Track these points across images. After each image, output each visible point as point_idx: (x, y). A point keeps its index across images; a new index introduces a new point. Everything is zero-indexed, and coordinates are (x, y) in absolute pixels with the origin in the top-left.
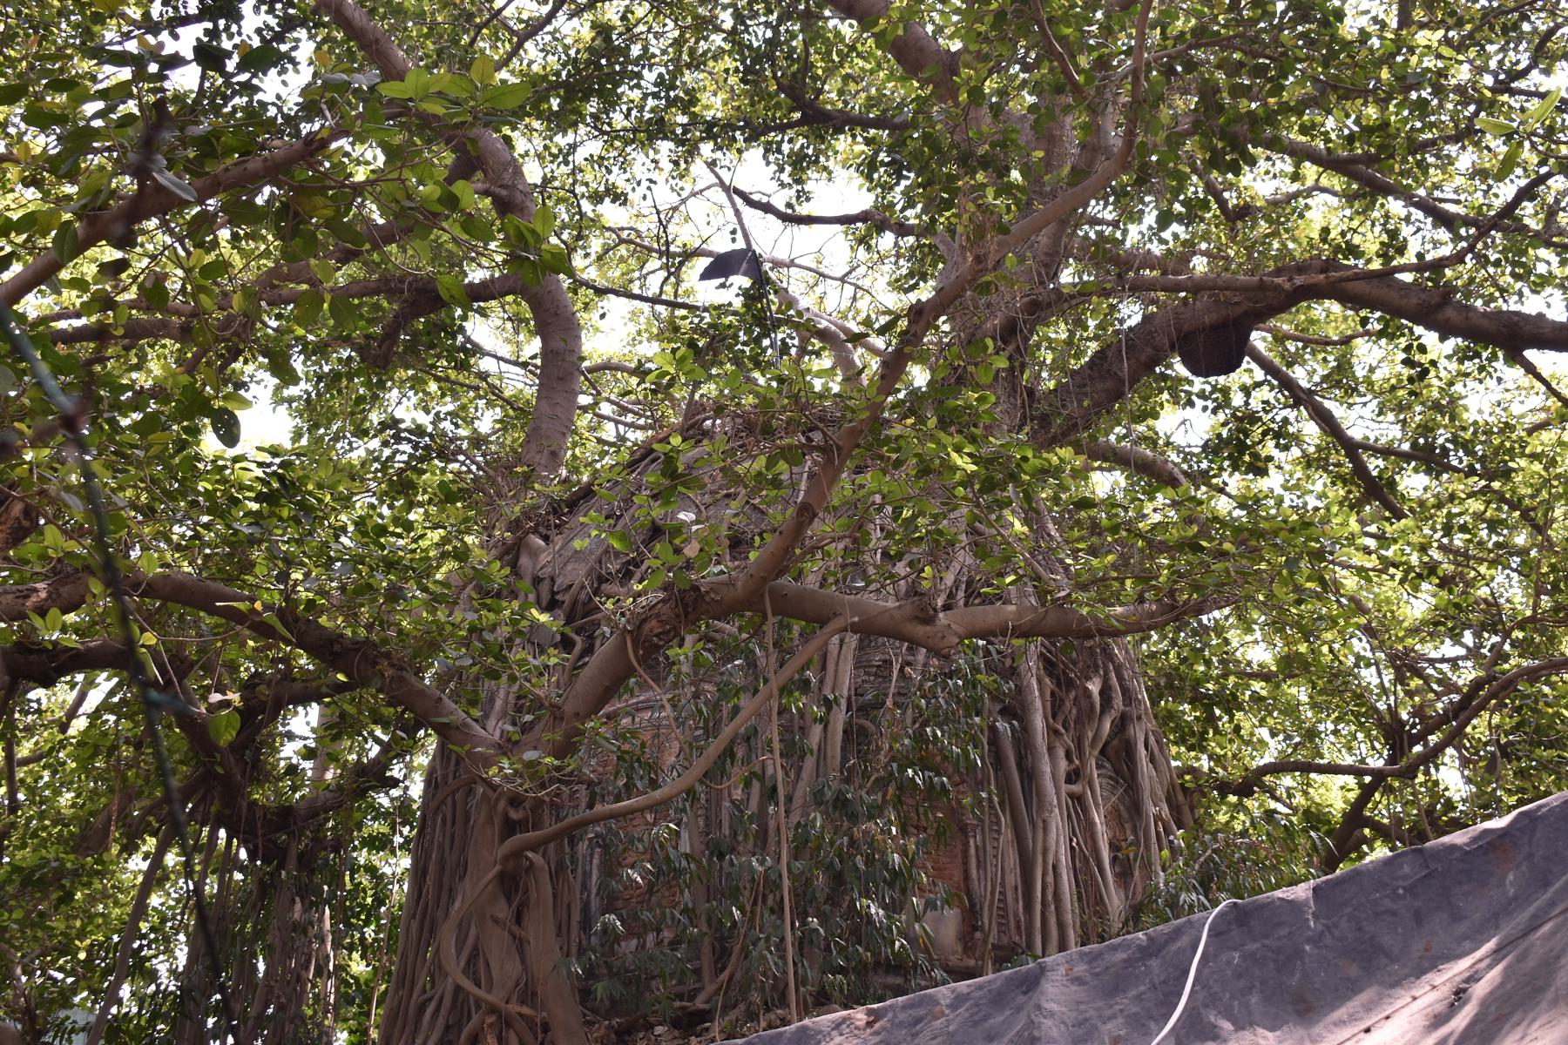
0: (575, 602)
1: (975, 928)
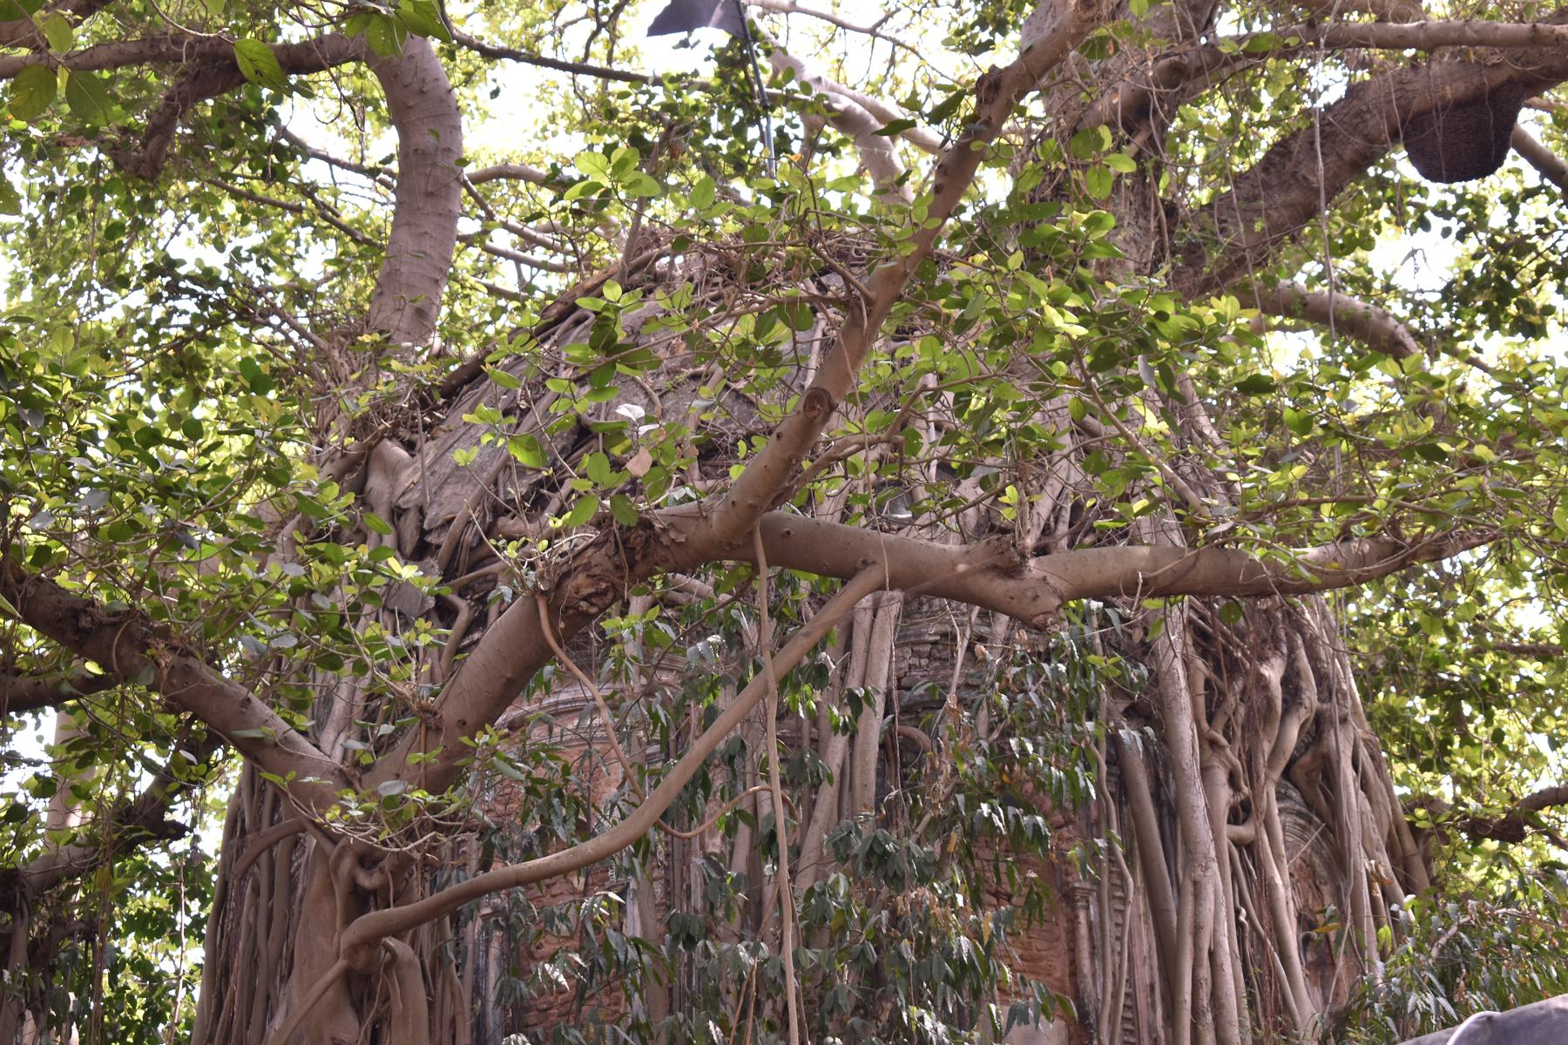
0: (457, 546)
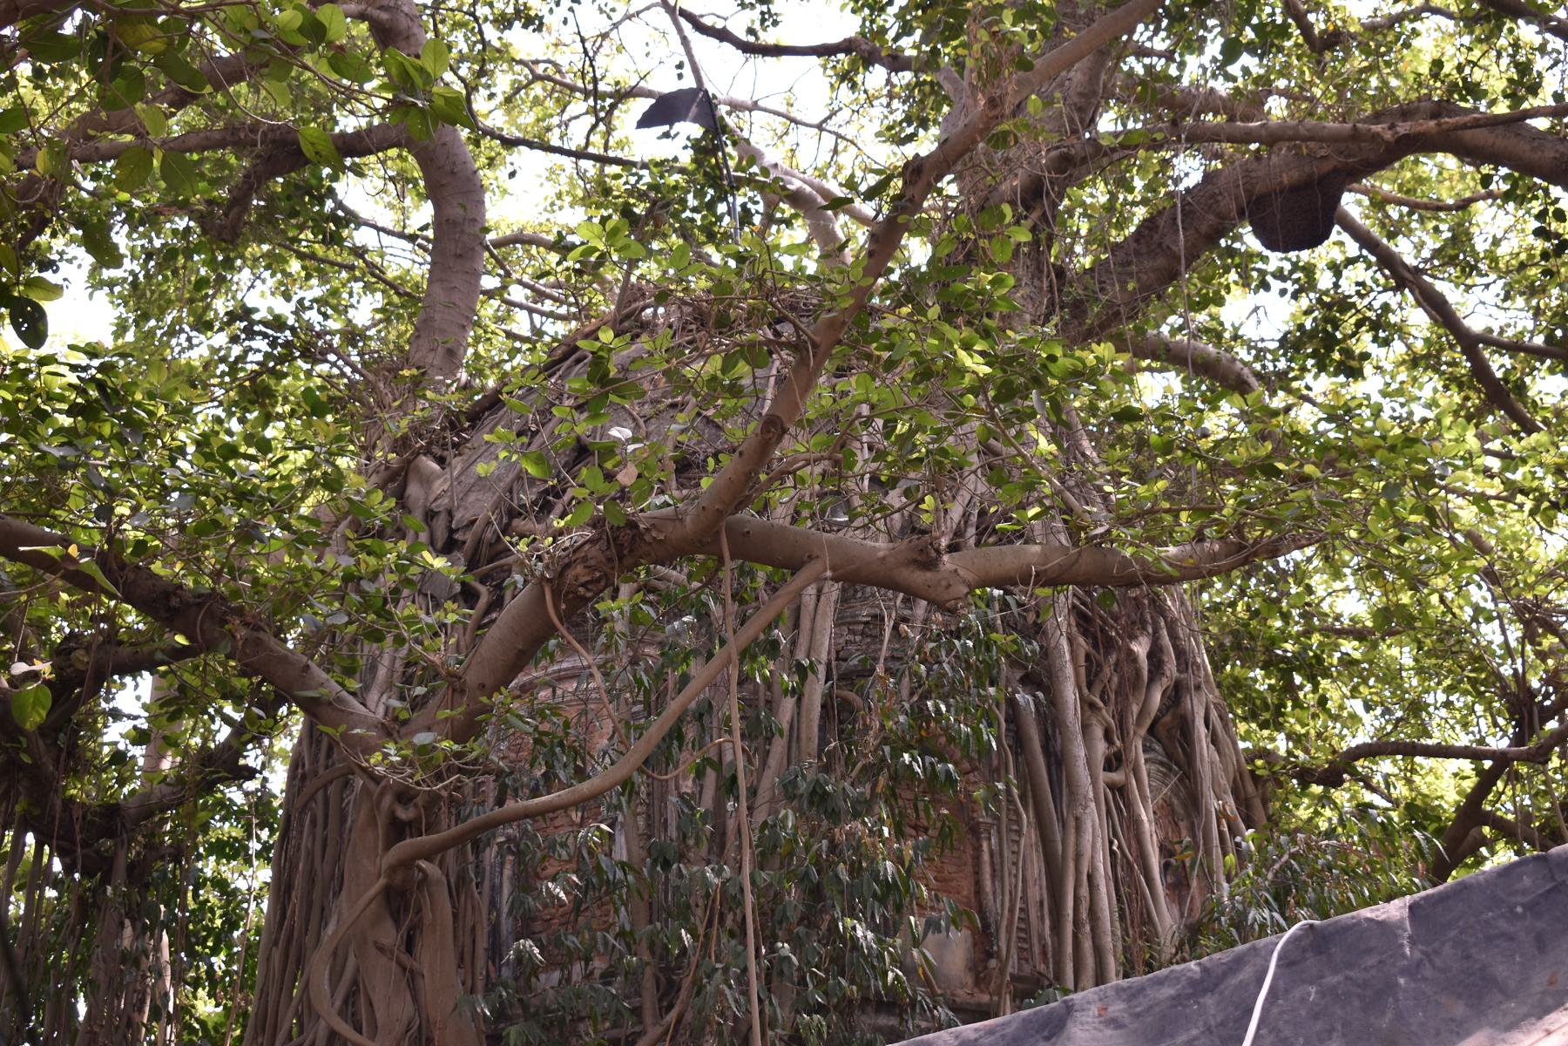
0: (479, 542)
1: (990, 955)
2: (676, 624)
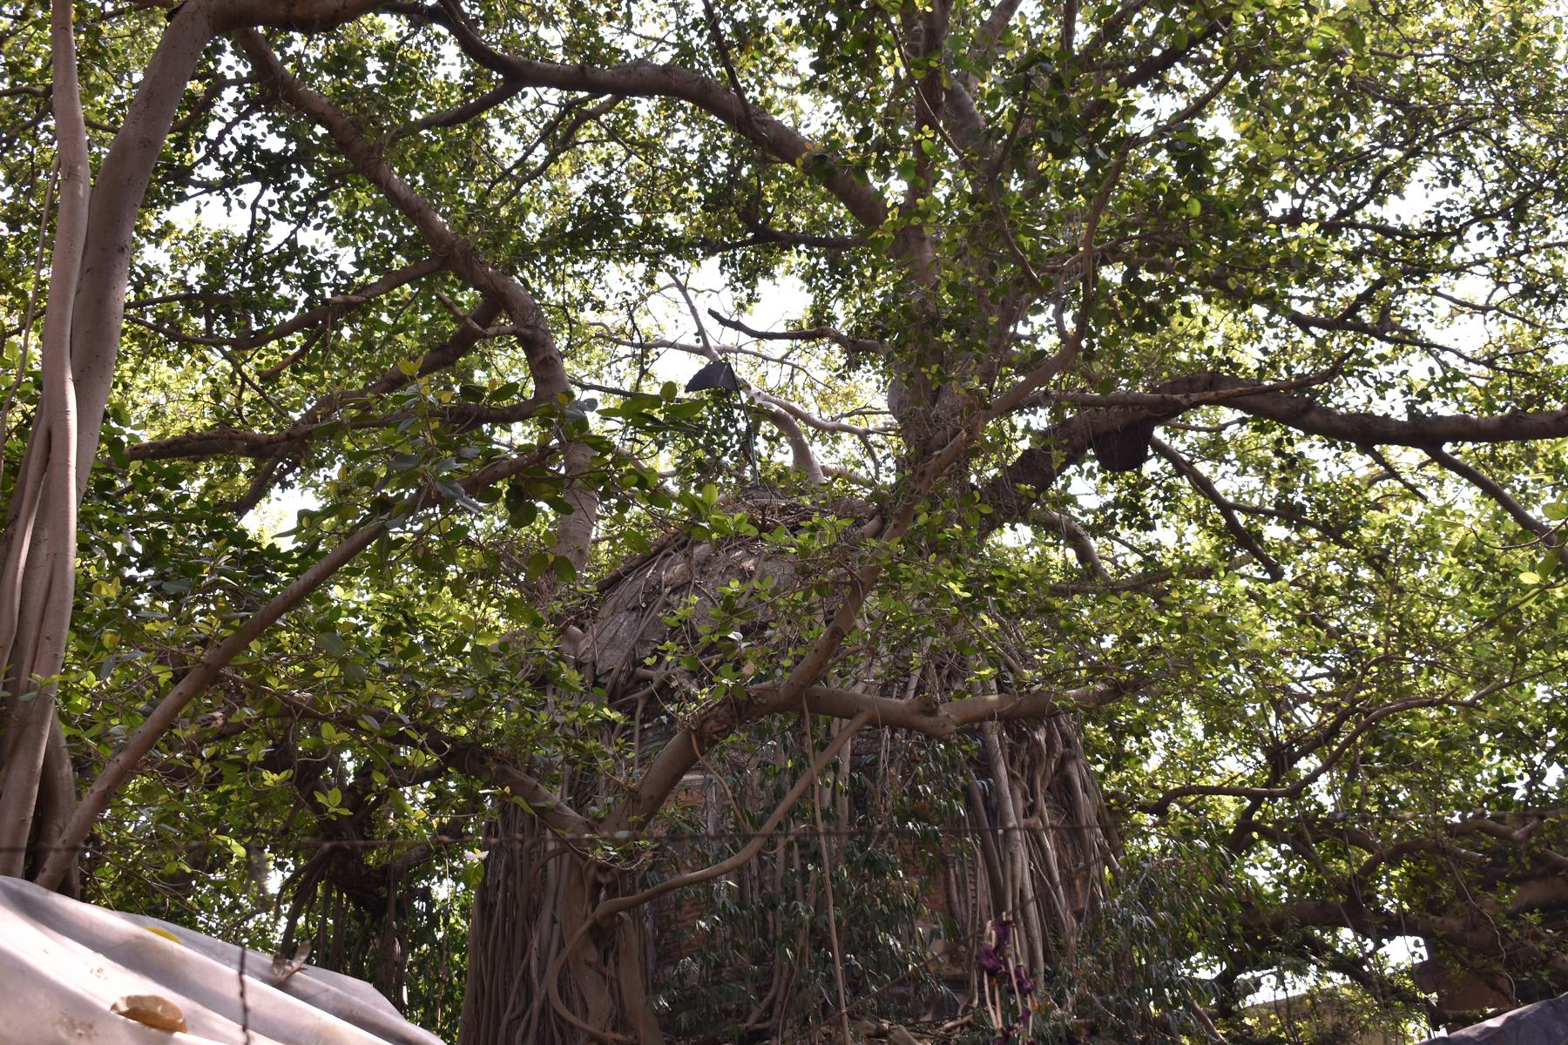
0: (615, 684)
2: (309, 407)
